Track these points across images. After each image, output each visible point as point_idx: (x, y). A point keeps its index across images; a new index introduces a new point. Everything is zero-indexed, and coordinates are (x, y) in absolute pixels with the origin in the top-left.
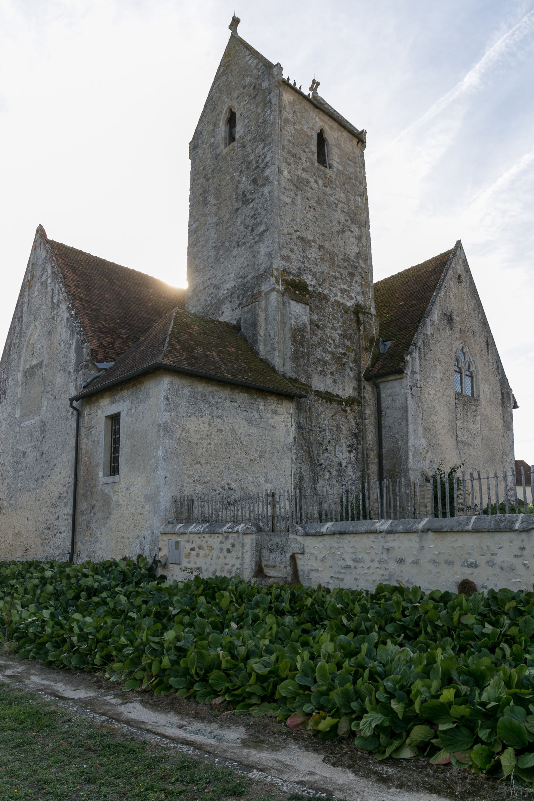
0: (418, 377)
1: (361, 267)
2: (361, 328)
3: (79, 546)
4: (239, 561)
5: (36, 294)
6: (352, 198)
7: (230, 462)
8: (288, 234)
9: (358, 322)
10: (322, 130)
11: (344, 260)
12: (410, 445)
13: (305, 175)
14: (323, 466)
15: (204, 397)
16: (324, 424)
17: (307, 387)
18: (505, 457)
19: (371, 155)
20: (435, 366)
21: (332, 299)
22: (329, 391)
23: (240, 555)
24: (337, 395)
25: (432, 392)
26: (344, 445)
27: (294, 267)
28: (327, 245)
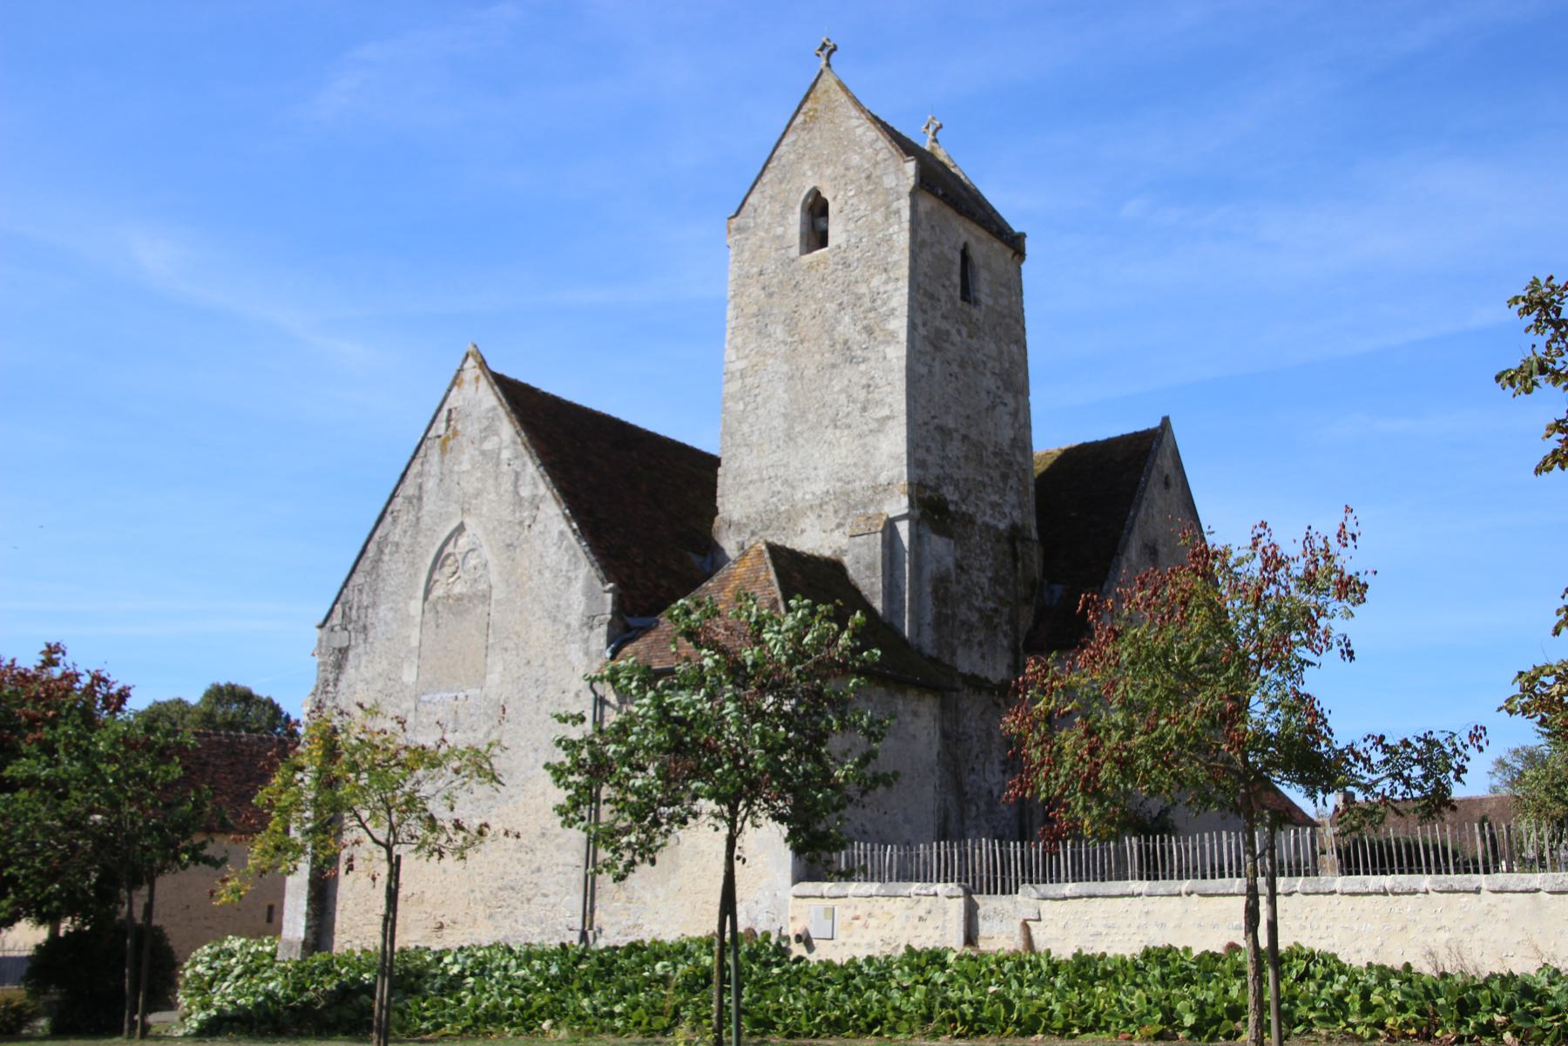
2: (1020, 565)
3: (600, 917)
4: (938, 932)
5: (466, 466)
6: (1005, 348)
9: (1015, 557)
10: (966, 245)
11: (995, 454)
13: (945, 325)
17: (951, 670)
19: (1031, 272)
21: (979, 522)
23: (940, 923)
24: (987, 680)
28: (973, 434)
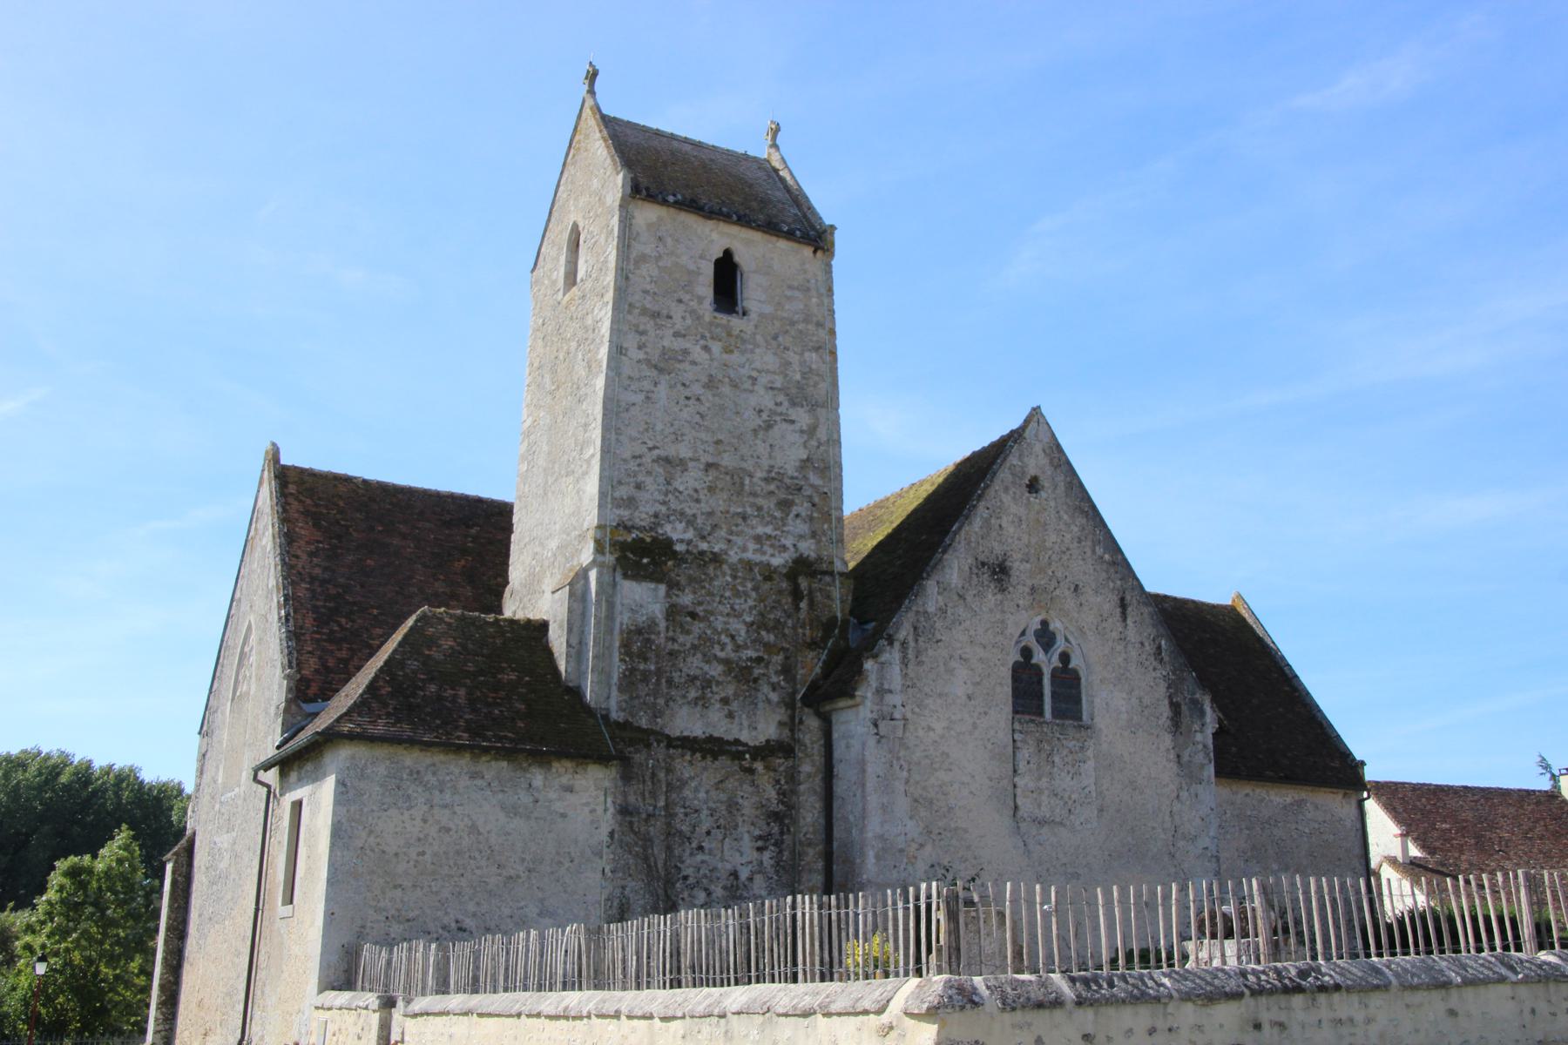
0: (896, 699)
1: (812, 486)
6: (794, 358)
7: (464, 882)
8: (635, 457)
10: (728, 254)
12: (870, 835)
14: (691, 880)
15: (416, 775)
16: (696, 798)
18: (1181, 844)
20: (951, 671)
22: (716, 735)
24: (737, 742)
25: (939, 727)
26: (746, 837)
27: (642, 516)
